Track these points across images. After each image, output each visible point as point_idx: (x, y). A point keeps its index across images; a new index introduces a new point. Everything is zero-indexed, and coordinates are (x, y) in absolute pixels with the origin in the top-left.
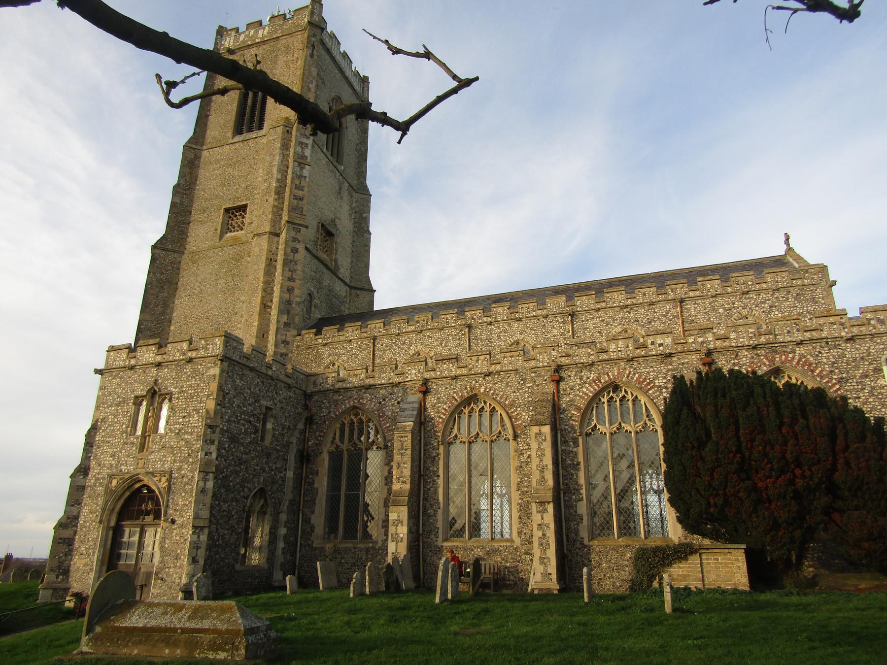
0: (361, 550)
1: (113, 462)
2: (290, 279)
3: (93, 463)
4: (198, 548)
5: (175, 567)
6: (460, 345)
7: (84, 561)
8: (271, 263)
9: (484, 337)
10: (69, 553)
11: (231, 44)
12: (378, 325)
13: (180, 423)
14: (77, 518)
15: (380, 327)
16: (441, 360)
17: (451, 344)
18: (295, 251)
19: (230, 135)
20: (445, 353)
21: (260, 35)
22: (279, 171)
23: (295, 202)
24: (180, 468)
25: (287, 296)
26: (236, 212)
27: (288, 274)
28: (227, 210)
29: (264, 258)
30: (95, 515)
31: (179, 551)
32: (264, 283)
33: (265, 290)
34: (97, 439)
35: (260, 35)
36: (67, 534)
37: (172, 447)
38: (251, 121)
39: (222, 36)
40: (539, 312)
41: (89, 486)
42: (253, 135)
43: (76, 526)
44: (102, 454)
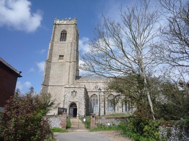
8: (70, 67)
19: (59, 41)
28: (60, 56)
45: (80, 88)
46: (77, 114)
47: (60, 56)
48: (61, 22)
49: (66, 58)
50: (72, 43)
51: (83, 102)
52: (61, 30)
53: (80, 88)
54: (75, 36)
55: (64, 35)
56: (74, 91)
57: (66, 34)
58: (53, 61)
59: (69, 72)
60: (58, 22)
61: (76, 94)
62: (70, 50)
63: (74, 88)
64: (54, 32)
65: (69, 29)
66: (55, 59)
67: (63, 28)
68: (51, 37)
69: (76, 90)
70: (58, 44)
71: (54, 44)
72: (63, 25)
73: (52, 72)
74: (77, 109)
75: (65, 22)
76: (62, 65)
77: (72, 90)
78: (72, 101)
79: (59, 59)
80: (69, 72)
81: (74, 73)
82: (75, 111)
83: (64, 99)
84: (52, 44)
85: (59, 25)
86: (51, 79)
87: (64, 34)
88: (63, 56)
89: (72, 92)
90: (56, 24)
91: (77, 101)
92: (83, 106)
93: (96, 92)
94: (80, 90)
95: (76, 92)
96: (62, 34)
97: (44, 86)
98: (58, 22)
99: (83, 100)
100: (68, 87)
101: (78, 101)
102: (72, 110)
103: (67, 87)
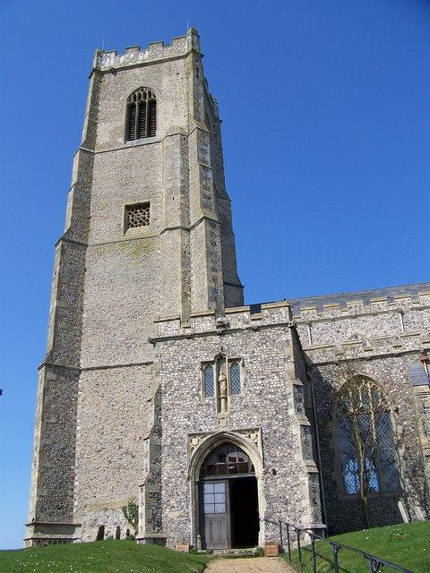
0: (387, 499)
1: (189, 423)
2: (214, 270)
3: (165, 425)
4: (315, 492)
5: (287, 511)
6: (395, 327)
7: (177, 514)
8: (185, 256)
9: (416, 320)
10: (159, 507)
11: (112, 64)
12: (311, 311)
13: (260, 385)
14: (159, 474)
15: (314, 313)
16: (379, 342)
17: (386, 327)
18: (214, 244)
19: (121, 140)
20: (381, 334)
21: (141, 57)
22: (182, 172)
23: (205, 200)
24: (269, 425)
25: (213, 284)
26: (137, 212)
27: (211, 265)
28: (128, 208)
29: (179, 249)
30: (180, 471)
31: (287, 497)
32: (183, 273)
33: (183, 280)
34: (164, 402)
35: (141, 57)
36: (154, 489)
37: (255, 407)
38: (140, 130)
39: (101, 57)
40: (391, 308)
41: (166, 446)
42: (144, 141)
43: (160, 482)
44: (174, 416)
45: (257, 329)
46: (257, 520)
47: (128, 208)
48: (122, 59)
49: (164, 212)
50: (184, 137)
51: (296, 430)
52: (129, 92)
53: (257, 329)
54: (196, 104)
55: (141, 116)
56: (220, 359)
57: (153, 103)
58: (94, 238)
59: (186, 283)
60: (109, 62)
61: (234, 373)
62: (178, 172)
63: (216, 338)
64: (95, 102)
65: (166, 80)
66: (105, 225)
67: (135, 80)
68: (88, 88)
69: (232, 344)
70: (114, 153)
71: (97, 158)
72: (137, 71)
73: (93, 298)
74: (254, 481)
75: (145, 56)
76: (147, 249)
77: (204, 351)
78: (212, 427)
79: (128, 225)
80: (186, 283)
81: (215, 280)
82: (243, 495)
83: (158, 421)
84: (85, 155)
85: (113, 71)
86: (87, 331)
87: (142, 105)
88: (146, 206)
89: (207, 364)
90: (99, 73)
91: (245, 425)
92: (298, 457)
93: (399, 355)
94: (264, 341)
95: (234, 361)
96: (131, 108)
97: (52, 376)
98: (109, 62)
99: (292, 411)
100: (175, 333)
101: (254, 425)
102: (217, 496)
103: (170, 333)
